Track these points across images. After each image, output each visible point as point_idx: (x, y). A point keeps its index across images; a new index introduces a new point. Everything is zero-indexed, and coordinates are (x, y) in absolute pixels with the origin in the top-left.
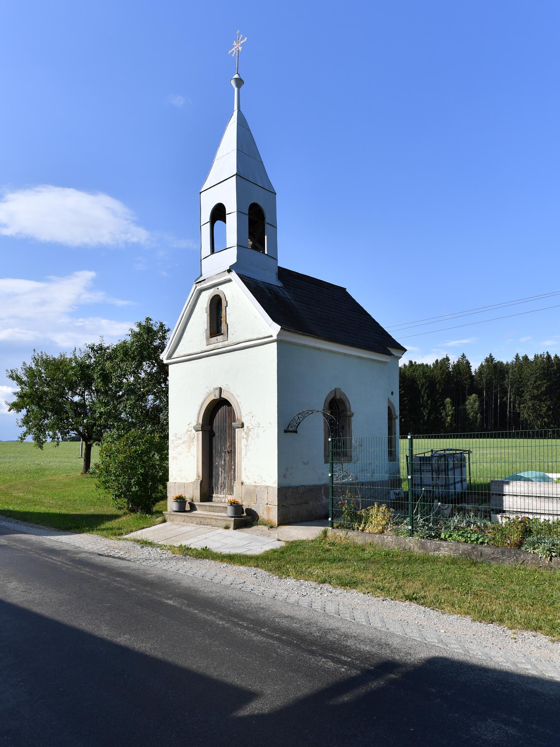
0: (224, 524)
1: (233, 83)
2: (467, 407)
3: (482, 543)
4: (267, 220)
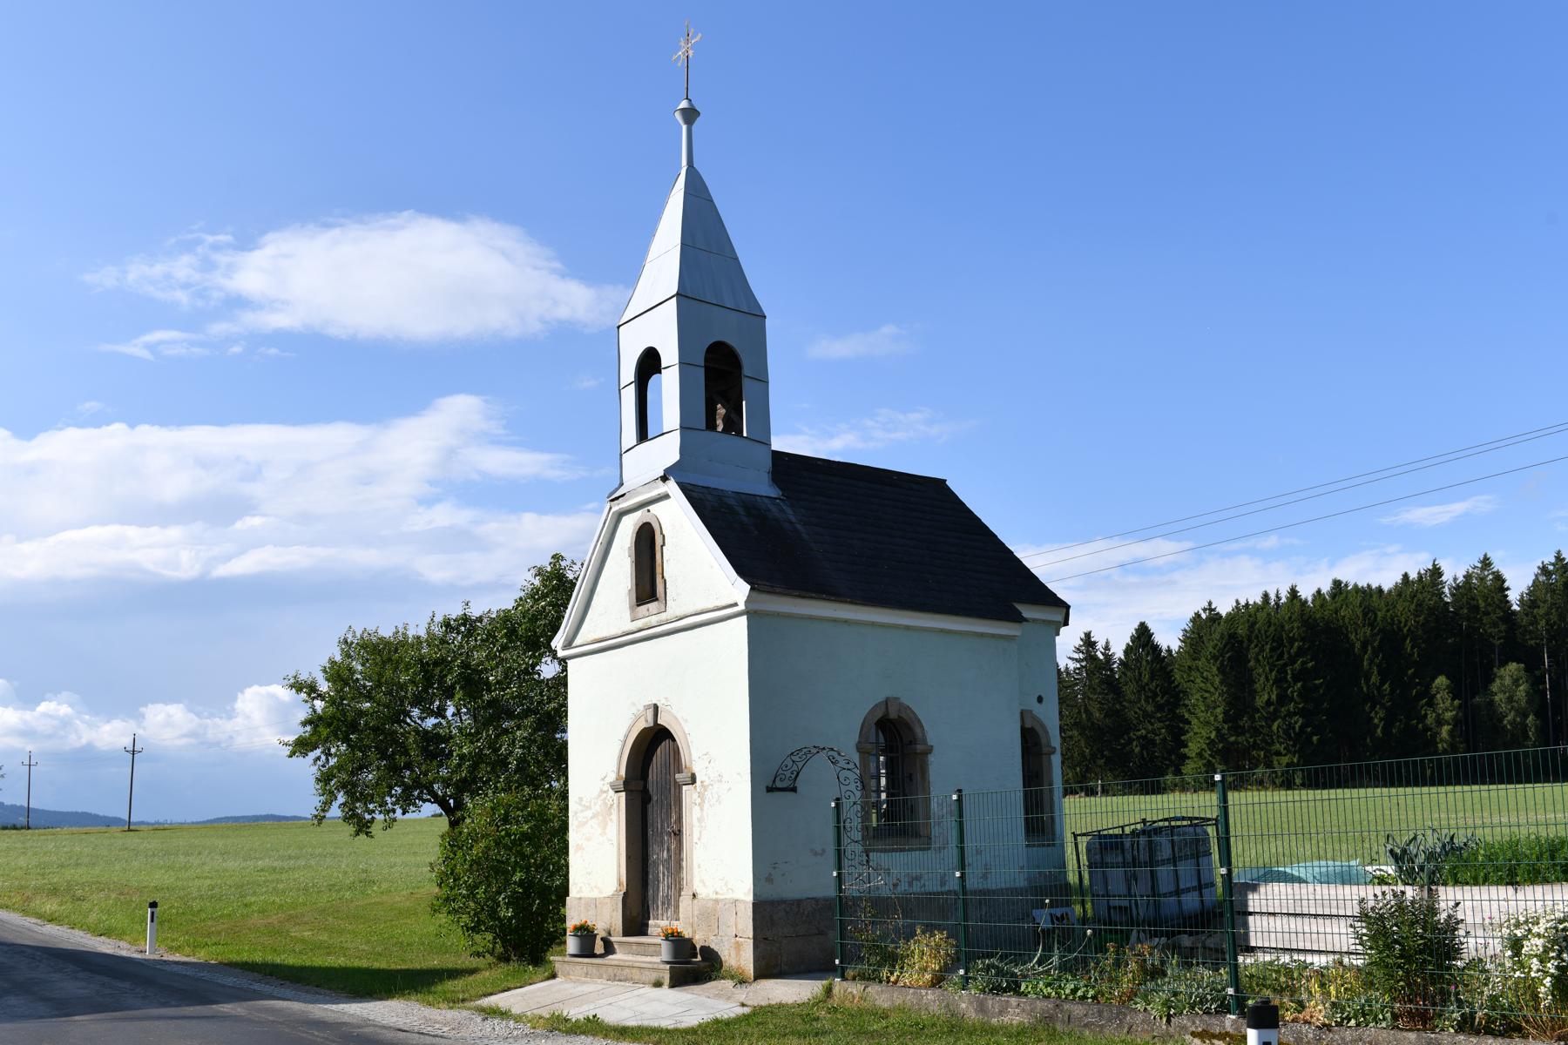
0: (654, 976)
1: (678, 116)
2: (1497, 698)
3: (1084, 997)
4: (746, 371)
